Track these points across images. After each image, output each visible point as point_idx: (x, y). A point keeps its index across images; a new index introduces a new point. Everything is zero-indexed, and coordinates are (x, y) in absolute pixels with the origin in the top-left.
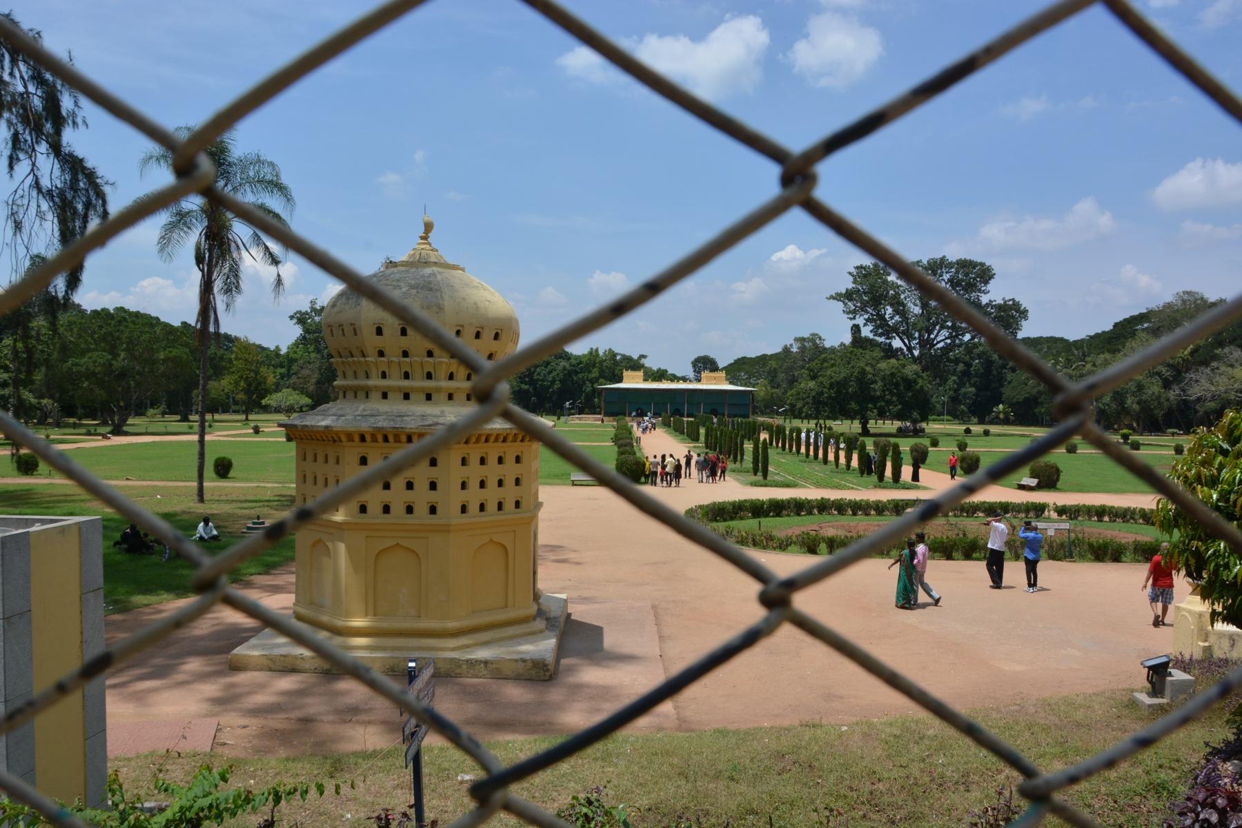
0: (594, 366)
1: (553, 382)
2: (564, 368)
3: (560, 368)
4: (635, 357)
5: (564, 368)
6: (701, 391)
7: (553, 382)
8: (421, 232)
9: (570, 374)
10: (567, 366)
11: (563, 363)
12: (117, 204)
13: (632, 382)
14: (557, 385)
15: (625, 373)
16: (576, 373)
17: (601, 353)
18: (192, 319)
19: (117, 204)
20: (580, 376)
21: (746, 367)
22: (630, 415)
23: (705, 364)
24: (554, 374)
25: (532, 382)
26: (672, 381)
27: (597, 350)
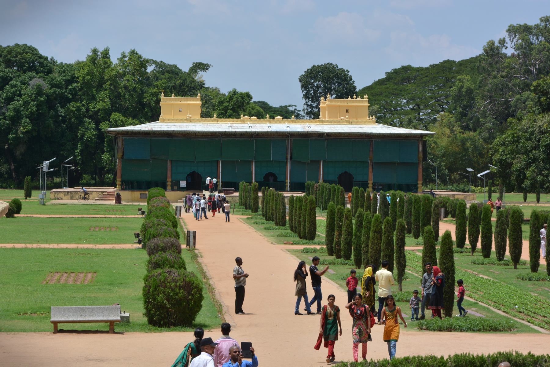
0: (100, 86)
1: (16, 119)
2: (39, 92)
3: (30, 90)
5: (39, 92)
7: (16, 119)
11: (37, 81)
13: (179, 117)
14: (25, 126)
15: (165, 102)
16: (65, 101)
17: (114, 59)
20: (72, 106)
22: (175, 186)
24: (17, 103)
26: (260, 116)
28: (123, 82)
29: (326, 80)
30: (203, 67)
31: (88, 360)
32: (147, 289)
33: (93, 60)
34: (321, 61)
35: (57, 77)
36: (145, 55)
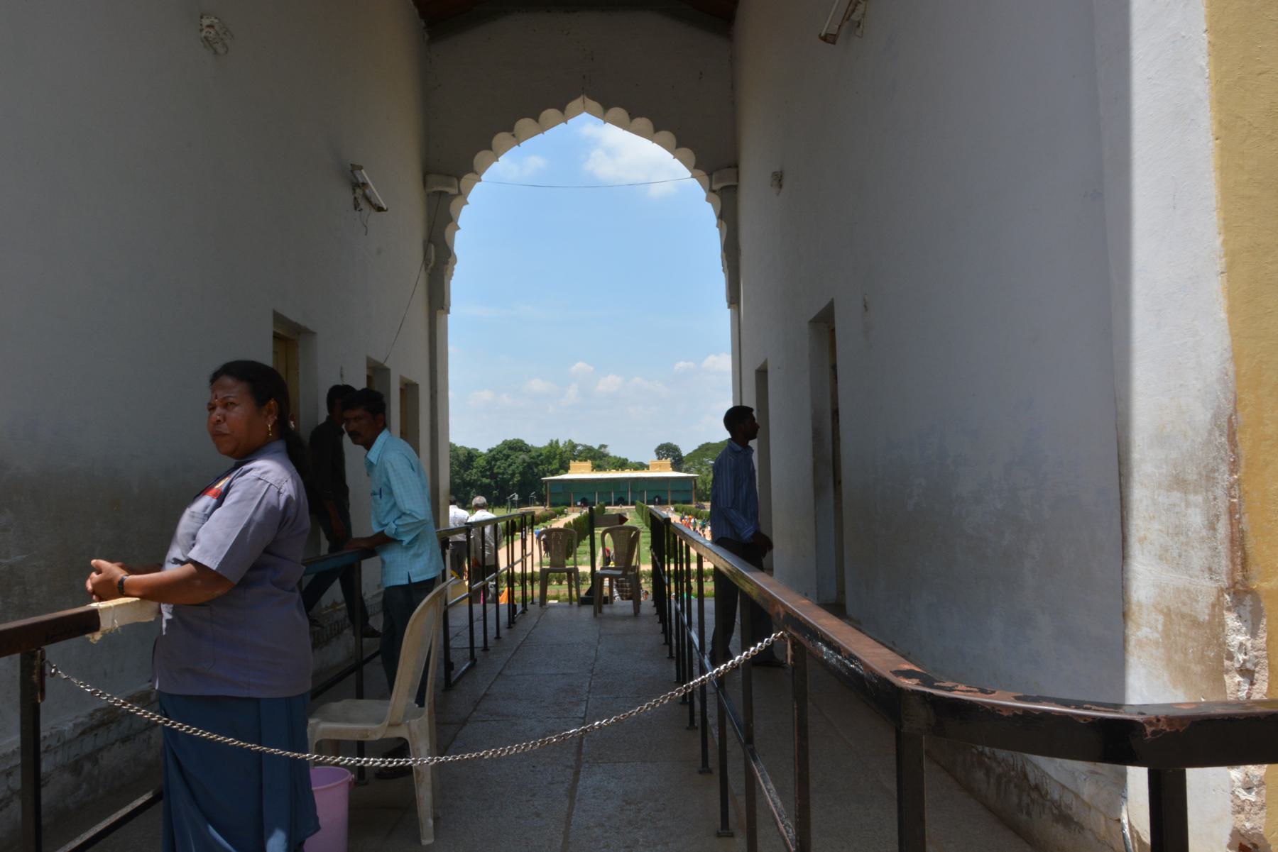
0: (554, 458)
1: (513, 475)
2: (524, 461)
3: (519, 460)
4: (596, 447)
5: (524, 461)
6: (644, 479)
7: (513, 475)
8: (346, 196)
9: (529, 466)
10: (527, 459)
11: (523, 456)
12: (379, 659)
13: (580, 472)
14: (517, 478)
15: (572, 464)
16: (537, 465)
17: (561, 444)
18: (1194, 776)
19: (379, 659)
20: (540, 468)
21: (710, 453)
22: (575, 505)
23: (668, 451)
24: (513, 467)
25: (493, 476)
26: (636, 469)
27: (557, 442)
28: (388, 449)
29: (668, 451)
30: (605, 446)
31: (1124, 558)
32: (1223, 529)
33: (551, 445)
34: (664, 442)
35: (533, 454)
36: (576, 442)
